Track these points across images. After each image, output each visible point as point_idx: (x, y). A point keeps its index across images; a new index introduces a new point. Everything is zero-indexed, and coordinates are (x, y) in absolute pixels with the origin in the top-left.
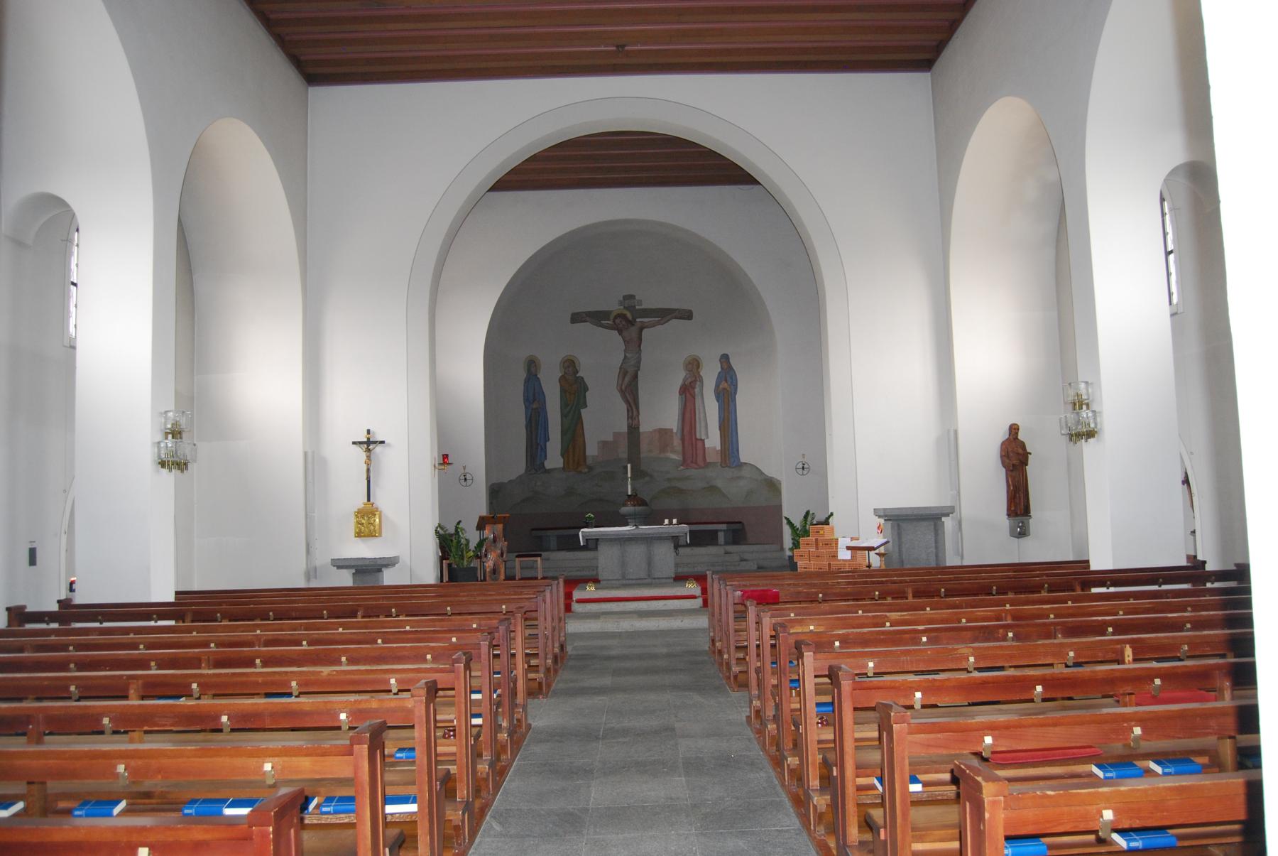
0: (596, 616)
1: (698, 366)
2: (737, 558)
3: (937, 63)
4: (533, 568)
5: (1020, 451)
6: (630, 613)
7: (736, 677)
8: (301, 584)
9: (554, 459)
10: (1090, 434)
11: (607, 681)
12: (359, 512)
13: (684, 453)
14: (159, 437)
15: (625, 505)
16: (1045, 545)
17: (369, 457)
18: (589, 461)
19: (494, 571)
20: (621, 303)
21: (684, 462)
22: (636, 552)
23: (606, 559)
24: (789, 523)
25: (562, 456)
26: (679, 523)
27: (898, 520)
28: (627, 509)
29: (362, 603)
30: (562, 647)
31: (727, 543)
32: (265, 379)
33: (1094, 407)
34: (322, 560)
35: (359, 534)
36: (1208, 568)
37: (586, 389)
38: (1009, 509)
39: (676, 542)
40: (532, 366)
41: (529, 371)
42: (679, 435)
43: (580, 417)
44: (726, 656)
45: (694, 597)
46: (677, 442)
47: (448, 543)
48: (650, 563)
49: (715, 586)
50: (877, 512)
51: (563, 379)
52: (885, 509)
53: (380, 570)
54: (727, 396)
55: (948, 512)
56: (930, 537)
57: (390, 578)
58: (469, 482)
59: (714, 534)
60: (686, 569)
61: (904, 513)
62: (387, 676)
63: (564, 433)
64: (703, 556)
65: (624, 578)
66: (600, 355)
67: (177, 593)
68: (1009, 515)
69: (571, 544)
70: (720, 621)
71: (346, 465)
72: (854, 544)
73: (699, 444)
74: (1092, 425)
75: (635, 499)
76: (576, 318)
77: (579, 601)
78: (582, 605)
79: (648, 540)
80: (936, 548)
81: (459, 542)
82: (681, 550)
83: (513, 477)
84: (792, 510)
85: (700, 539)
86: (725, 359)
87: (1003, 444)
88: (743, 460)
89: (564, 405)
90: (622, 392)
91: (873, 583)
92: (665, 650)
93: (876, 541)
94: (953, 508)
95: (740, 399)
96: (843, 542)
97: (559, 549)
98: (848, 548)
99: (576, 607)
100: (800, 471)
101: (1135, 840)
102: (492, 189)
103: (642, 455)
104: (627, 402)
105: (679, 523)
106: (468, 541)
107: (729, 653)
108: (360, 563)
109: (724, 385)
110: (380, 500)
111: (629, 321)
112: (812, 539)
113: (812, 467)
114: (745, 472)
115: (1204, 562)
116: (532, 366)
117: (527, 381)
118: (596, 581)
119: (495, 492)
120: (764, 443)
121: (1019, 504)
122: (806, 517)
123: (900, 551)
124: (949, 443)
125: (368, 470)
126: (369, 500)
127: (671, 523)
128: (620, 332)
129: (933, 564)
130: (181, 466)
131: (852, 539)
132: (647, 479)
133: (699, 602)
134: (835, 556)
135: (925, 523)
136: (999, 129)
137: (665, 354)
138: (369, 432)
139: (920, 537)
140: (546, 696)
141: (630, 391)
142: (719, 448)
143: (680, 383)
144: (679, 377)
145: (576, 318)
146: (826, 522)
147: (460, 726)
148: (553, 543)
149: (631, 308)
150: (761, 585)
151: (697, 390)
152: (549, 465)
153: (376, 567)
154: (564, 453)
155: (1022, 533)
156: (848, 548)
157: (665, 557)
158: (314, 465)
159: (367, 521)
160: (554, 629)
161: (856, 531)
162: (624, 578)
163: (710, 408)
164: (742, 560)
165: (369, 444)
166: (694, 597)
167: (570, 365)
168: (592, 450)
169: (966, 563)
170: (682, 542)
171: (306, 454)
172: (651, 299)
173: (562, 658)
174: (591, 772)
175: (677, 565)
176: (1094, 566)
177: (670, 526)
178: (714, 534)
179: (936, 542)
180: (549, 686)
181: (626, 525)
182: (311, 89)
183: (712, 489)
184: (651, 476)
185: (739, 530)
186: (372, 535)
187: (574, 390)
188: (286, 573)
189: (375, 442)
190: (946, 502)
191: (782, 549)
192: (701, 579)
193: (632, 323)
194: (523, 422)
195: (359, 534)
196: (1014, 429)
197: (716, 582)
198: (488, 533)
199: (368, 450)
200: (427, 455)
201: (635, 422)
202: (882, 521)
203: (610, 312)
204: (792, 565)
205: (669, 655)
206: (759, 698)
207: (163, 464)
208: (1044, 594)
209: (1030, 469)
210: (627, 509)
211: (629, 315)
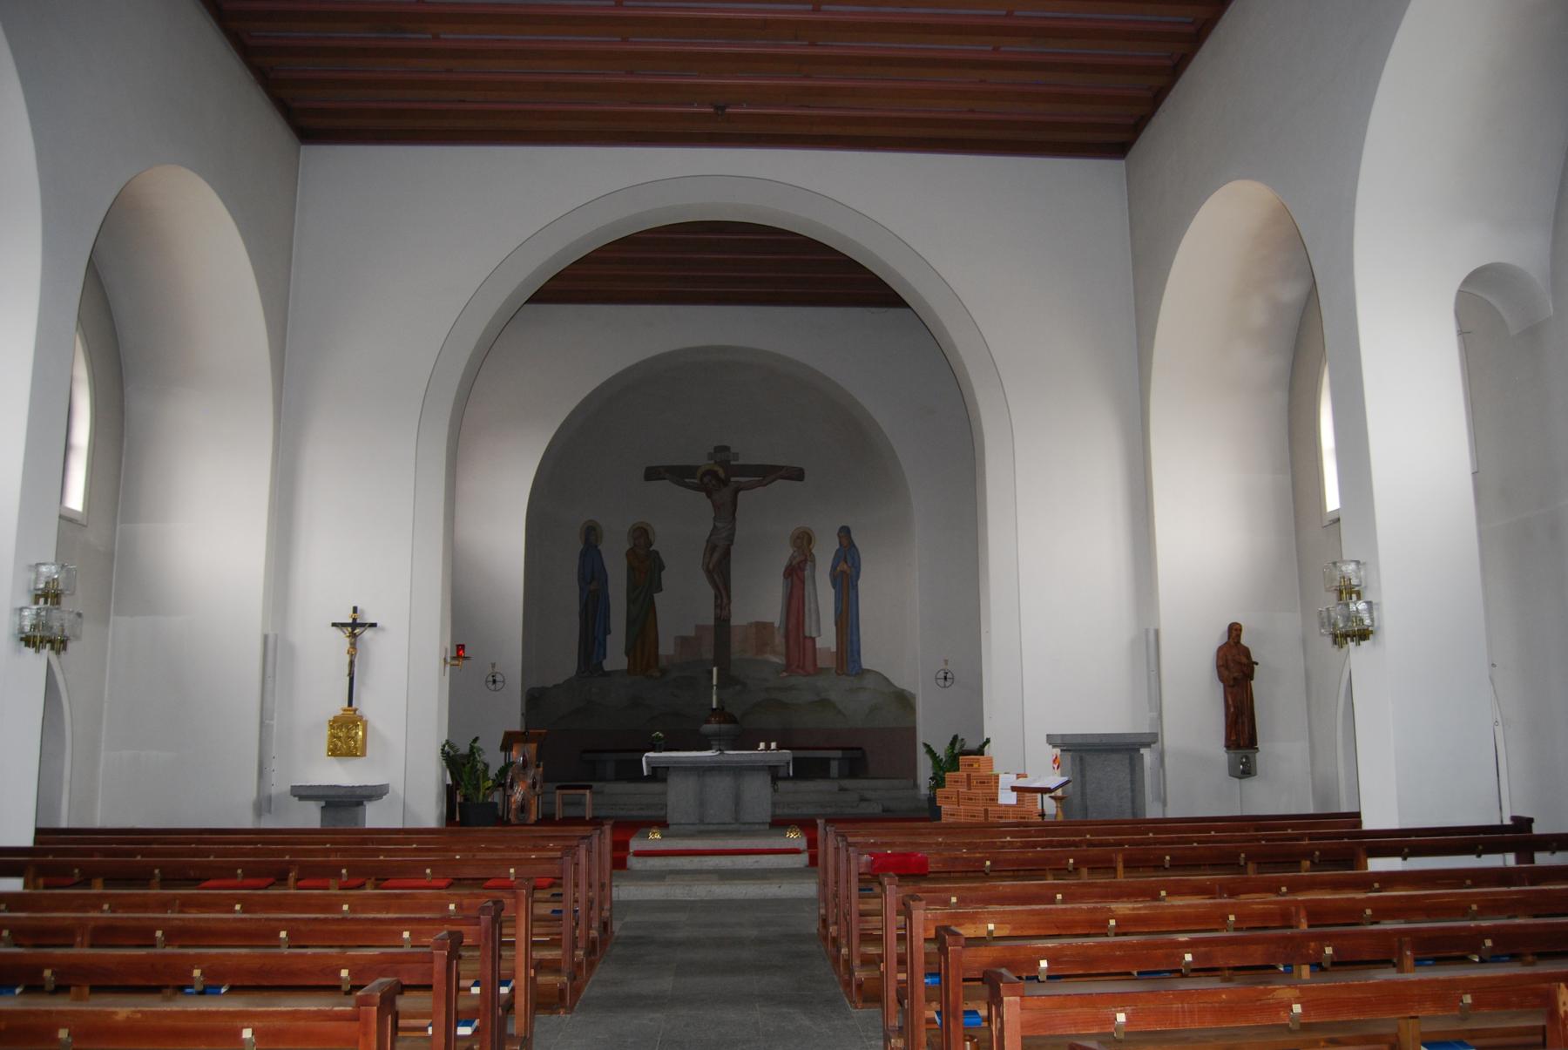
0: (659, 876)
1: (810, 541)
3: (1135, 147)
4: (580, 804)
5: (1244, 660)
6: (709, 872)
7: (860, 986)
8: (247, 821)
9: (616, 658)
10: (1363, 635)
11: (666, 983)
12: (336, 719)
14: (25, 600)
15: (708, 722)
16: (1282, 788)
17: (353, 645)
19: (523, 808)
20: (711, 456)
21: (788, 667)
22: (721, 786)
23: (679, 796)
24: (930, 751)
26: (779, 748)
27: (1080, 752)
28: (710, 728)
29: (332, 851)
30: (605, 926)
31: (841, 776)
32: (214, 531)
33: (1368, 596)
34: (280, 785)
35: (334, 752)
36: (1537, 829)
37: (661, 567)
38: (1228, 738)
39: (775, 774)
40: (591, 535)
41: (587, 541)
42: (782, 631)
43: (653, 603)
44: (844, 951)
45: (796, 851)
46: (779, 640)
47: (460, 764)
48: (737, 800)
49: (829, 840)
50: (1052, 740)
51: (631, 554)
52: (1063, 736)
53: (360, 804)
55: (1151, 740)
57: (375, 817)
58: (499, 685)
59: (826, 762)
60: (787, 811)
64: (811, 794)
65: (702, 822)
66: (681, 524)
67: (39, 832)
68: (1228, 747)
69: (631, 772)
70: (836, 896)
72: (1022, 783)
73: (809, 644)
74: (1367, 622)
75: (721, 714)
76: (652, 474)
77: (638, 854)
78: (641, 859)
79: (738, 770)
80: (1133, 790)
81: (474, 767)
82: (780, 784)
84: (932, 732)
85: (806, 769)
86: (845, 532)
87: (1220, 649)
90: (709, 573)
91: (1061, 844)
92: (754, 933)
93: (1053, 779)
94: (1155, 735)
95: (863, 585)
96: (1006, 780)
98: (1014, 789)
99: (634, 863)
100: (941, 682)
102: (544, 296)
103: (733, 657)
104: (716, 587)
106: (487, 766)
107: (849, 945)
108: (332, 793)
109: (843, 566)
110: (367, 705)
111: (721, 480)
112: (962, 774)
113: (962, 677)
115: (1531, 820)
116: (591, 535)
117: (583, 555)
118: (662, 824)
119: (534, 700)
120: (895, 644)
121: (1241, 731)
122: (953, 743)
123: (1083, 794)
124: (1149, 645)
125: (352, 664)
126: (350, 704)
127: (768, 747)
128: (709, 496)
129: (1128, 816)
130: (59, 644)
131: (1019, 776)
133: (803, 859)
136: (1221, 229)
137: (766, 523)
138: (355, 610)
140: (571, 1009)
141: (719, 571)
142: (834, 649)
143: (785, 562)
144: (784, 555)
145: (652, 474)
146: (980, 751)
150: (895, 842)
151: (807, 573)
152: (608, 665)
153: (343, 802)
155: (1245, 770)
156: (1014, 789)
157: (758, 795)
158: (275, 653)
159: (347, 736)
160: (590, 902)
161: (1023, 762)
162: (702, 822)
163: (824, 597)
164: (863, 799)
165: (355, 627)
166: (796, 851)
167: (641, 535)
168: (666, 648)
169: (1171, 814)
170: (782, 773)
171: (266, 638)
172: (751, 452)
173: (604, 943)
175: (775, 804)
176: (1368, 824)
177: (767, 752)
178: (826, 762)
179: (1133, 782)
180: (577, 991)
181: (708, 748)
182: (303, 148)
183: (825, 703)
185: (866, 766)
186: (351, 753)
187: (646, 569)
188: (223, 800)
189: (363, 625)
190: (1145, 729)
191: (915, 786)
192: (807, 825)
193: (725, 483)
194: (575, 607)
195: (334, 752)
196: (1235, 630)
197: (831, 837)
198: (517, 756)
199: (353, 636)
200: (434, 641)
202: (1057, 751)
203: (697, 468)
204: (935, 813)
206: (901, 1031)
207: (28, 641)
208: (1305, 871)
209: (1257, 685)
210: (710, 728)
211: (721, 473)
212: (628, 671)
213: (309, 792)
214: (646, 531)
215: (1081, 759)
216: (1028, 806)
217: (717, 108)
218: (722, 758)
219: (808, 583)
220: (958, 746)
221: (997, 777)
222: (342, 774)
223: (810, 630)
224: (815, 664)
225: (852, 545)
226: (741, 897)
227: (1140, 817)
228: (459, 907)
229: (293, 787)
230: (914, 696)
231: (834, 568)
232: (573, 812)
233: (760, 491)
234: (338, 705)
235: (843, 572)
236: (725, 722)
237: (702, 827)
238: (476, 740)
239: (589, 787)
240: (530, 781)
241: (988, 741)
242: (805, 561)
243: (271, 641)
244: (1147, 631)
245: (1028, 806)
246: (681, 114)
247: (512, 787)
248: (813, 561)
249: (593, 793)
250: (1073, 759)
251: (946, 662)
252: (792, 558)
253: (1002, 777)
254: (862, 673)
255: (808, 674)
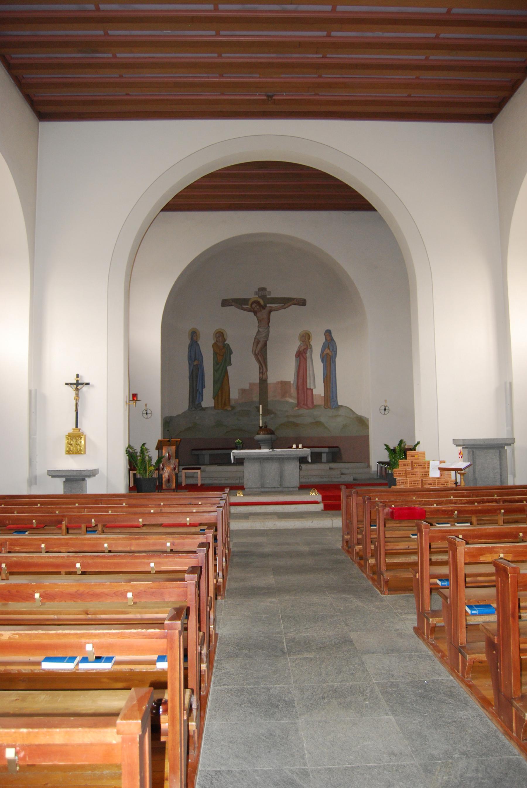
1: (309, 337)
2: (339, 473)
8: (24, 491)
9: (208, 400)
11: (270, 580)
13: (298, 398)
15: (258, 434)
17: (77, 395)
18: (232, 403)
19: (169, 481)
20: (256, 293)
21: (298, 404)
22: (272, 468)
23: (250, 473)
25: (214, 398)
26: (303, 447)
27: (472, 448)
28: (260, 437)
31: (328, 462)
34: (41, 470)
37: (231, 352)
39: (302, 460)
40: (194, 335)
41: (192, 339)
42: (295, 386)
43: (226, 372)
46: (293, 391)
47: (135, 460)
48: (281, 476)
50: (456, 443)
51: (215, 345)
53: (84, 480)
54: (329, 359)
56: (496, 462)
57: (92, 487)
58: (149, 415)
61: (479, 443)
62: (83, 641)
63: (215, 382)
65: (262, 487)
66: (241, 330)
69: (225, 461)
71: (62, 399)
72: (443, 466)
73: (309, 392)
75: (265, 429)
76: (225, 303)
79: (281, 459)
80: (501, 469)
83: (180, 413)
85: (316, 458)
86: (328, 333)
88: (340, 404)
89: (216, 363)
90: (256, 355)
92: (306, 549)
93: (462, 464)
97: (211, 464)
98: (440, 469)
100: (383, 412)
101: (475, 610)
102: (170, 207)
103: (269, 400)
104: (259, 362)
105: (303, 447)
109: (327, 351)
110: (85, 426)
111: (262, 306)
112: (408, 461)
114: (341, 412)
116: (194, 335)
117: (190, 346)
118: (241, 488)
125: (77, 405)
126: (77, 426)
127: (297, 447)
128: (255, 314)
129: (498, 484)
131: (441, 462)
132: (272, 416)
134: (427, 474)
135: (491, 451)
137: (286, 330)
138: (78, 376)
139: (489, 461)
141: (261, 354)
142: (323, 395)
144: (295, 345)
145: (225, 303)
147: (173, 699)
148: (207, 459)
149: (263, 297)
151: (308, 355)
153: (74, 479)
154: (216, 396)
157: (293, 473)
158: (36, 399)
159: (75, 443)
161: (441, 455)
163: (317, 367)
164: (342, 474)
165: (78, 385)
167: (220, 336)
168: (234, 395)
171: (30, 392)
172: (277, 291)
174: (289, 704)
182: (40, 123)
183: (318, 423)
184: (275, 414)
186: (78, 453)
187: (223, 353)
189: (82, 384)
191: (369, 466)
193: (264, 307)
194: (187, 374)
199: (77, 390)
200: (121, 395)
201: (264, 376)
203: (248, 300)
205: (312, 554)
210: (260, 437)
211: (262, 302)
212: (215, 407)
213: (57, 474)
214: (222, 333)
215: (473, 452)
216: (446, 478)
217: (268, 96)
218: (273, 453)
219: (308, 360)
220: (402, 445)
221: (428, 463)
222: (73, 464)
223: (310, 385)
224: (313, 402)
225: (332, 339)
226: (291, 527)
227: (505, 485)
228: (173, 544)
229: (49, 471)
230: (368, 420)
231: (322, 352)
232: (191, 481)
233: (282, 311)
234: (70, 427)
235: (327, 354)
236: (268, 434)
237: (263, 490)
238: (144, 444)
239: (199, 469)
240: (172, 466)
241: (418, 443)
242: (307, 348)
243: (33, 392)
244: (505, 383)
245: (446, 478)
246: (249, 100)
247: (163, 469)
248: (311, 348)
249: (201, 471)
250: (469, 453)
251: (386, 401)
252: (300, 347)
253: (431, 463)
254: (339, 407)
255: (309, 408)
